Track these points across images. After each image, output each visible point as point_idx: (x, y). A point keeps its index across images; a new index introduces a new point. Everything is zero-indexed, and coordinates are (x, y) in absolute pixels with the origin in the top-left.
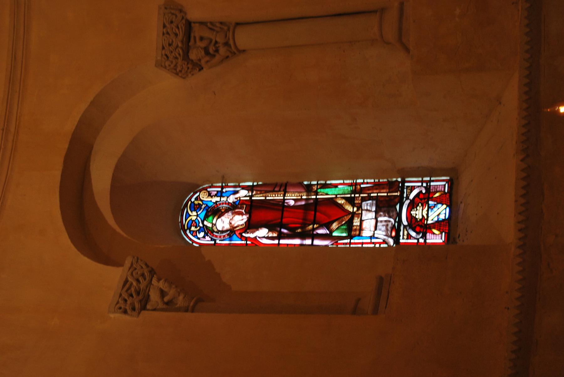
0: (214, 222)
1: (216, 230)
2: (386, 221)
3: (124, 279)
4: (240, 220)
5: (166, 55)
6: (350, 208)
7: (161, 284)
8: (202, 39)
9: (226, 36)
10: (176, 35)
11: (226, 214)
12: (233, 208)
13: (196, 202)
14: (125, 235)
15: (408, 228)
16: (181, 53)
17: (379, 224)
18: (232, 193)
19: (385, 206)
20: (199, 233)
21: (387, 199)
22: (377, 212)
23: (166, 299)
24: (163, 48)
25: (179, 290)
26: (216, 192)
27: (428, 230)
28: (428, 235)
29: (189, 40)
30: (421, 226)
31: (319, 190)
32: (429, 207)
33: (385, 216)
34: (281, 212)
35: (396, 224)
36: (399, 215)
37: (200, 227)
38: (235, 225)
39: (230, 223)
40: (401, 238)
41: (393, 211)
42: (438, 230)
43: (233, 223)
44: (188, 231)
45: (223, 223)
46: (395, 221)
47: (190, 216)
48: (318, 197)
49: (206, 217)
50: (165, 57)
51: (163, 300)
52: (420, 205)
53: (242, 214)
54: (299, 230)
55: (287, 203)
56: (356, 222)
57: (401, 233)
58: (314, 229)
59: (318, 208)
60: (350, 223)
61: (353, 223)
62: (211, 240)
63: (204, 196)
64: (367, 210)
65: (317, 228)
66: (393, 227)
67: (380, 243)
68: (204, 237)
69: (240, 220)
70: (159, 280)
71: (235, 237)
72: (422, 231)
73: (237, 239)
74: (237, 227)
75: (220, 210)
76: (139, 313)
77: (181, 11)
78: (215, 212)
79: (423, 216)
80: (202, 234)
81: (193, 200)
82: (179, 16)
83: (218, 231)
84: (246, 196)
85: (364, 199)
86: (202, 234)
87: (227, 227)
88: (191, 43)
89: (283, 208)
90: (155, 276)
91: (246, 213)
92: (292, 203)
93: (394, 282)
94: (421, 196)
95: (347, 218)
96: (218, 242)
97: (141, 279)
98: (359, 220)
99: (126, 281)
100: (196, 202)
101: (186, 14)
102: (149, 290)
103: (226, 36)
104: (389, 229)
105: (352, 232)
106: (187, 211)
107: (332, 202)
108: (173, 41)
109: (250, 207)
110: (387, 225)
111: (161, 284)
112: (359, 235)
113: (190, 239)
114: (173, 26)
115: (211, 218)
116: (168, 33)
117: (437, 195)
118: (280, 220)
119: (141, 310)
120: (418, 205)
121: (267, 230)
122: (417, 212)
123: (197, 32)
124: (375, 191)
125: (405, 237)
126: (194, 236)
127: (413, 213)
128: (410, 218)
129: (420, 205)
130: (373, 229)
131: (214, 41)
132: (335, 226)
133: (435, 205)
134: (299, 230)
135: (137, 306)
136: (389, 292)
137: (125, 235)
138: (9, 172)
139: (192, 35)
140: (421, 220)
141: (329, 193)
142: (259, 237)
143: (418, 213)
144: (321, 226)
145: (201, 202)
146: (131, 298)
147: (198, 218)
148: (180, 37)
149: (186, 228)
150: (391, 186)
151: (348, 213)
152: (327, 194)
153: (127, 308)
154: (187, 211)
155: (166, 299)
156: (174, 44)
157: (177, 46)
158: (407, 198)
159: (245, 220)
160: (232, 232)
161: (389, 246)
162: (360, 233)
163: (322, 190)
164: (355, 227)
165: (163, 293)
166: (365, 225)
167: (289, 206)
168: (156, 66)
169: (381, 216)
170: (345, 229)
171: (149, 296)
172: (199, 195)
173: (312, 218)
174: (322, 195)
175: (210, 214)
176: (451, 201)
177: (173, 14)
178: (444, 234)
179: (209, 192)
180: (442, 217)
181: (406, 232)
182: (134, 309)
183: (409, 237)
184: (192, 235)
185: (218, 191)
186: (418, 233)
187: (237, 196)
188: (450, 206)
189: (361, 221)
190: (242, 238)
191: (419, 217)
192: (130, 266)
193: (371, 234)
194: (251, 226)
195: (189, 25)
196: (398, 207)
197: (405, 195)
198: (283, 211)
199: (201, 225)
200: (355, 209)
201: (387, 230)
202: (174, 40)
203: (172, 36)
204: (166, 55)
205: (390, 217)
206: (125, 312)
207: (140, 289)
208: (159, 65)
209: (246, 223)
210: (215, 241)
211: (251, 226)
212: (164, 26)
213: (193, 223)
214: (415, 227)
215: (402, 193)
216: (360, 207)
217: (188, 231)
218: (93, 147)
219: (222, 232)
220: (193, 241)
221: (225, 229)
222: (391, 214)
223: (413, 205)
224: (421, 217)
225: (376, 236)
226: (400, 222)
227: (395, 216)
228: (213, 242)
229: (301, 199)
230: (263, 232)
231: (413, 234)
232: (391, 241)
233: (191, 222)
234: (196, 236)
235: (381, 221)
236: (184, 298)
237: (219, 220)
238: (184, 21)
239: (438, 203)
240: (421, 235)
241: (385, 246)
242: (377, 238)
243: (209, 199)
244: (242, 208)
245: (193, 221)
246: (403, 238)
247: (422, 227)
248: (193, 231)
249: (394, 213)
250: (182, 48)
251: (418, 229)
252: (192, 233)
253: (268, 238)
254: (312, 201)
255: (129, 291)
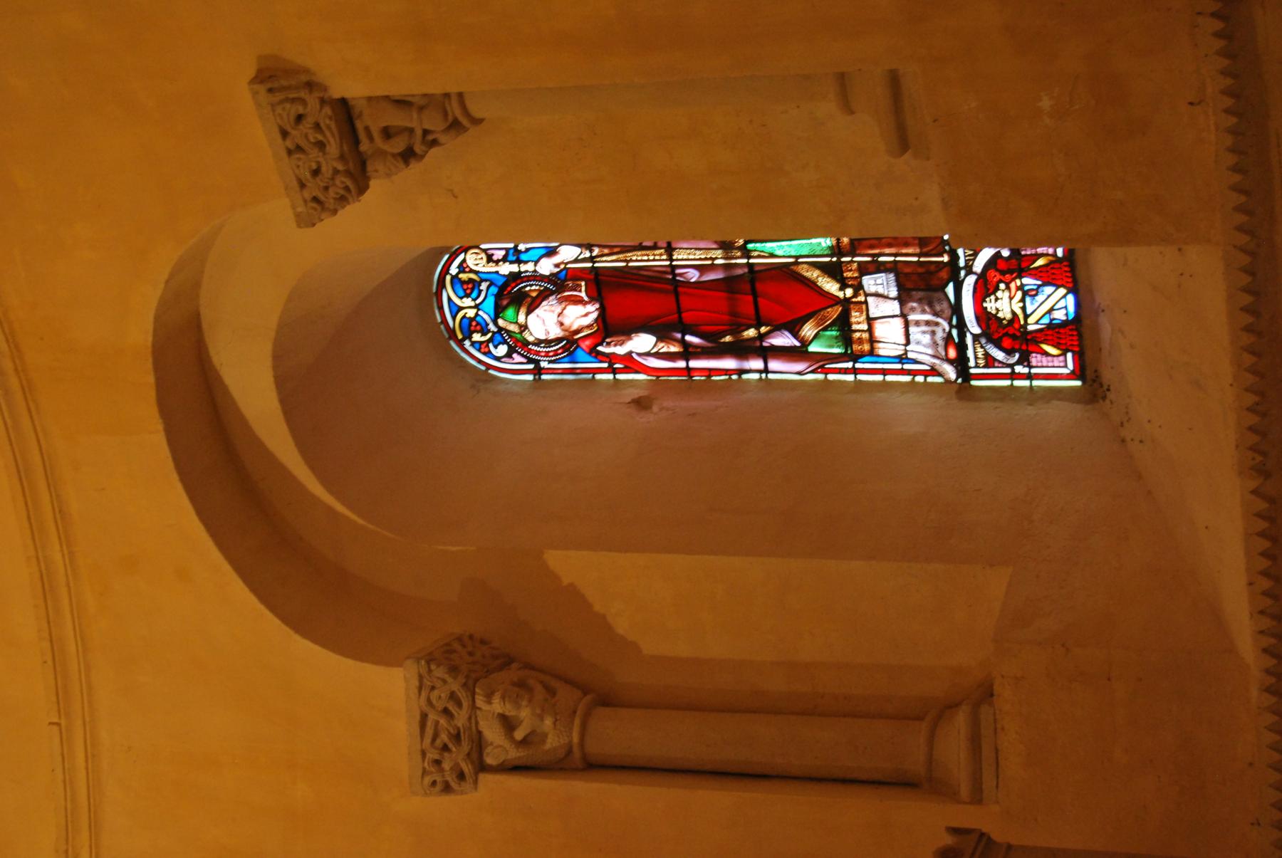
0: (521, 318)
1: (531, 339)
2: (928, 323)
3: (418, 718)
4: (581, 316)
5: (315, 199)
6: (831, 287)
7: (498, 706)
8: (387, 133)
9: (446, 114)
10: (321, 145)
11: (544, 303)
12: (559, 284)
13: (463, 276)
14: (360, 521)
15: (983, 341)
16: (349, 183)
17: (912, 329)
18: (543, 252)
19: (921, 286)
20: (496, 347)
21: (920, 270)
22: (902, 299)
23: (519, 735)
24: (302, 185)
25: (538, 711)
26: (503, 253)
27: (1031, 348)
28: (1035, 358)
29: (357, 142)
30: (1014, 337)
31: (750, 246)
32: (1025, 293)
33: (924, 312)
34: (673, 299)
35: (955, 332)
36: (957, 308)
37: (494, 333)
38: (575, 327)
39: (562, 324)
40: (972, 363)
41: (939, 300)
42: (1056, 346)
43: (567, 322)
44: (467, 343)
45: (544, 323)
46: (951, 326)
47: (461, 308)
48: (751, 261)
49: (499, 311)
50: (314, 205)
51: (512, 739)
52: (1002, 286)
53: (578, 301)
54: (728, 339)
55: (681, 275)
56: (858, 322)
57: (970, 353)
58: (762, 337)
59: (759, 287)
60: (843, 323)
61: (850, 325)
62: (528, 363)
63: (474, 260)
64: (877, 295)
65: (767, 334)
66: (948, 339)
67: (925, 374)
68: (509, 355)
69: (581, 316)
70: (489, 697)
71: (580, 354)
72: (1017, 347)
73: (589, 358)
74: (577, 332)
75: (526, 295)
76: (476, 782)
77: (310, 85)
78: (514, 294)
79: (1014, 313)
80: (502, 350)
81: (454, 270)
82: (312, 101)
83: (538, 342)
84: (576, 261)
85: (864, 270)
86: (502, 350)
87: (556, 332)
88: (365, 146)
89: (676, 287)
90: (477, 690)
91: (592, 299)
92: (693, 276)
93: (1003, 729)
94: (1001, 265)
95: (835, 312)
96: (544, 364)
97: (452, 707)
98: (864, 316)
99: (424, 717)
100: (463, 276)
101: (325, 89)
102: (477, 723)
103: (446, 114)
104: (941, 342)
105: (855, 347)
106: (449, 299)
107: (787, 273)
108: (319, 164)
109: (600, 285)
110: (933, 333)
111: (498, 706)
112: (872, 353)
113: (480, 361)
114: (306, 126)
115: (510, 312)
116: (299, 149)
117: (1040, 262)
118: (676, 316)
119: (476, 774)
120: (997, 289)
121: (652, 339)
122: (999, 304)
123: (371, 121)
124: (887, 251)
125: (982, 362)
126: (485, 354)
127: (990, 305)
128: (984, 317)
129: (1002, 286)
130: (898, 332)
131: (419, 132)
132: (808, 330)
133: (1039, 286)
134: (728, 339)
135: (467, 768)
136: (997, 751)
137: (360, 521)
138: (43, 442)
139: (359, 126)
140: (1011, 322)
141: (778, 253)
142: (639, 355)
143: (1003, 304)
144: (777, 328)
145: (472, 276)
146: (446, 754)
147: (480, 313)
148: (333, 148)
149: (460, 337)
150: (929, 244)
151: (834, 300)
152: (772, 256)
153: (449, 779)
154: (449, 299)
155: (519, 735)
156: (326, 171)
157: (336, 172)
158: (969, 271)
159: (595, 315)
160: (569, 343)
161: (948, 381)
162: (872, 349)
163: (758, 246)
164: (857, 335)
165: (508, 724)
166: (880, 330)
167: (687, 284)
168: (299, 226)
169: (913, 309)
170: (836, 337)
171: (480, 733)
172: (464, 261)
173: (751, 311)
174: (759, 257)
175: (505, 302)
176: (1075, 282)
177: (293, 100)
178: (1069, 355)
179: (485, 251)
180: (1059, 315)
181: (980, 352)
182: (461, 776)
183: (990, 361)
184: (479, 350)
185: (507, 250)
186: (1009, 352)
187: (556, 259)
188: (1073, 290)
189: (870, 321)
190: (594, 352)
191: (1005, 314)
192: (417, 683)
193: (899, 351)
194: (609, 327)
195: (344, 110)
196: (950, 290)
197: (962, 263)
198: (676, 293)
199: (492, 327)
200: (849, 292)
201: (935, 344)
202: (321, 159)
203: (314, 153)
204: (315, 199)
205: (936, 314)
206: (447, 789)
207: (458, 729)
208: (305, 222)
209: (596, 320)
210: (537, 362)
211: (609, 327)
212: (285, 134)
213: (472, 326)
214: (1000, 339)
215: (954, 257)
216: (858, 288)
217: (467, 343)
218: (198, 315)
219: (548, 342)
220: (489, 367)
221: (552, 336)
222: (938, 308)
223: (984, 289)
224: (1009, 316)
225: (910, 355)
226: (962, 326)
227: (948, 312)
228: (531, 366)
229: (713, 267)
230: (642, 343)
231: (999, 355)
232: (951, 372)
233: (466, 321)
234: (488, 353)
235: (917, 323)
236: (554, 723)
237: (532, 317)
238: (327, 110)
239: (1046, 284)
240: (1017, 356)
241: (938, 380)
242: (915, 362)
243: (492, 268)
244: (577, 288)
245: (472, 320)
246: (977, 366)
247: (1014, 338)
248: (481, 343)
249: (945, 305)
250: (348, 173)
251: (1007, 343)
252: (479, 346)
253: (658, 355)
254: (740, 272)
255: (438, 743)
